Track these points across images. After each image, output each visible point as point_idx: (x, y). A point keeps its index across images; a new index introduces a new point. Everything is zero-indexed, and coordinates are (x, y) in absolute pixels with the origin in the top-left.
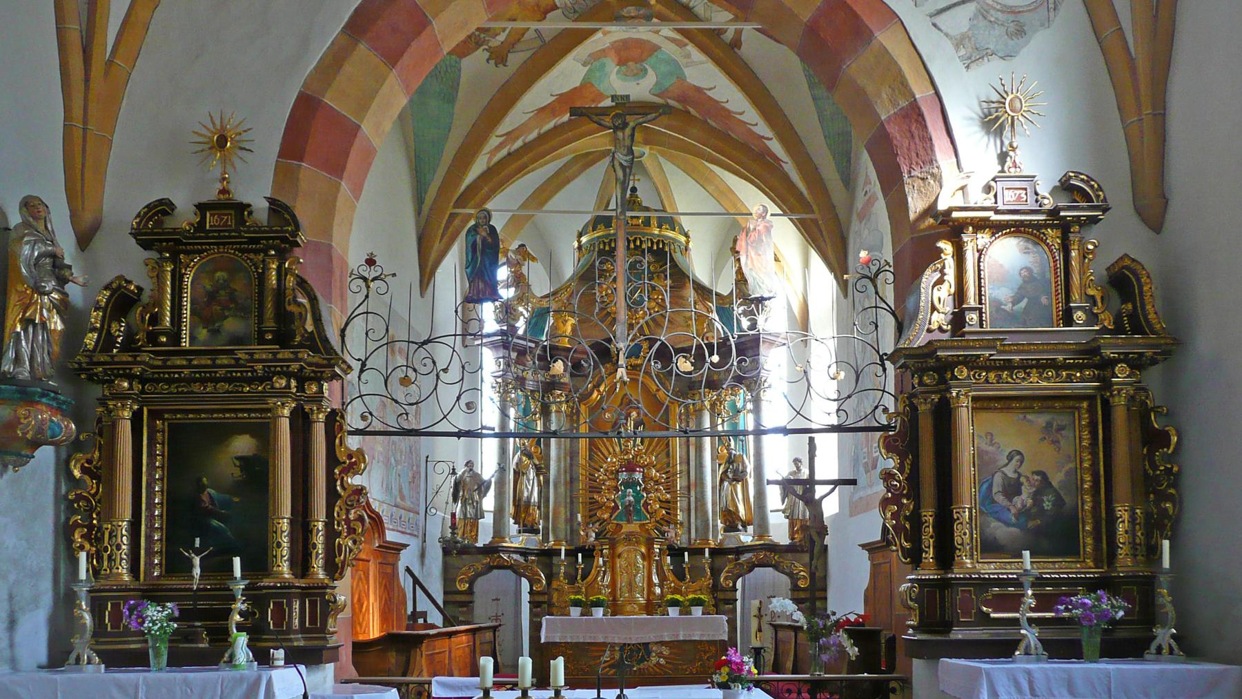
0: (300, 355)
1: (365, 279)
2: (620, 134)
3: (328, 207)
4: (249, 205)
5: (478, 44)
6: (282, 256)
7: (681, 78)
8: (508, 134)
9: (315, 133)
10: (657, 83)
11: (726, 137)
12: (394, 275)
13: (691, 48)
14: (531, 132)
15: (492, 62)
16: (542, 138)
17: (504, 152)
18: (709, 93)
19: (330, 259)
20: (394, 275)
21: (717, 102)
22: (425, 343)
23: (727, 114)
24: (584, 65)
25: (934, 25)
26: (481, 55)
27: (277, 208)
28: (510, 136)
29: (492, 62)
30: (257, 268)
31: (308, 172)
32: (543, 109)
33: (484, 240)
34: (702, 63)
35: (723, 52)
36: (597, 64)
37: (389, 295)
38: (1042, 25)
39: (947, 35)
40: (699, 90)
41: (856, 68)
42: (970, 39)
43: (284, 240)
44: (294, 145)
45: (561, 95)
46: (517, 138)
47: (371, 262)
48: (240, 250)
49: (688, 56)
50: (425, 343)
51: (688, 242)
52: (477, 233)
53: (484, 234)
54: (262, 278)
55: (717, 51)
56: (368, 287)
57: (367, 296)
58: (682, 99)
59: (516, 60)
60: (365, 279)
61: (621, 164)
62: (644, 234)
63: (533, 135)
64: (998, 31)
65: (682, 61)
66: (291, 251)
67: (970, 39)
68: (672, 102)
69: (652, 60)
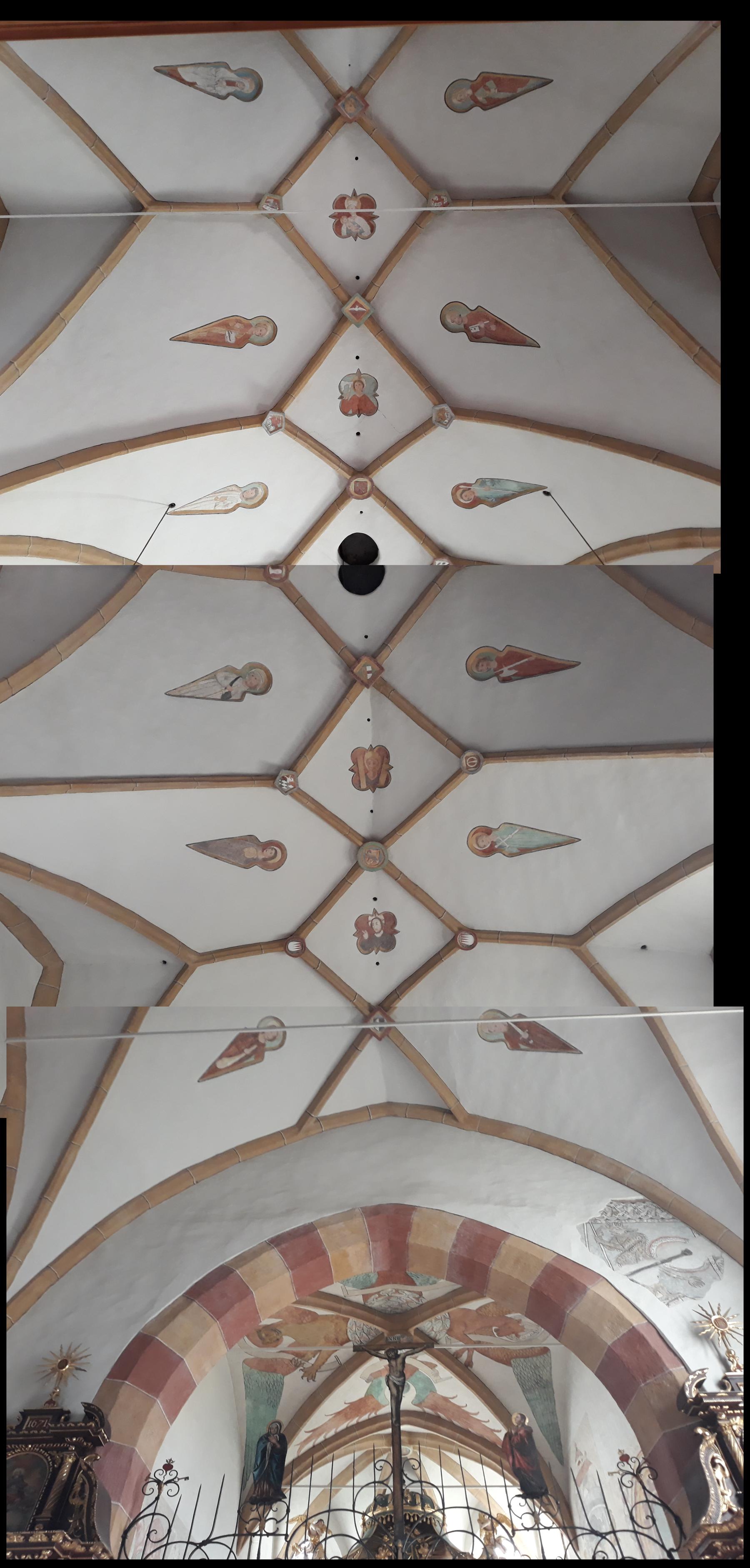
0: (54, 1538)
1: (159, 1482)
2: (393, 1363)
3: (139, 1420)
4: (69, 1412)
5: (297, 1366)
6: (82, 1451)
7: (433, 1391)
8: (313, 1431)
9: (147, 1363)
10: (417, 1396)
11: (466, 1433)
12: (187, 1478)
13: (440, 1368)
14: (330, 1429)
15: (305, 1378)
16: (338, 1436)
17: (310, 1445)
18: (452, 1401)
19: (130, 1461)
20: (187, 1478)
21: (459, 1407)
22: (205, 1543)
23: (467, 1415)
24: (367, 1381)
25: (632, 1280)
26: (298, 1373)
27: (92, 1412)
28: (315, 1432)
29: (305, 1378)
30: (54, 1463)
31: (128, 1390)
32: (339, 1413)
33: (274, 1447)
34: (448, 1378)
35: (463, 1370)
36: (376, 1381)
37: (178, 1496)
38: (715, 1278)
39: (644, 1286)
40: (446, 1399)
41: (578, 1312)
42: (663, 1288)
43: (87, 1437)
44: (123, 1368)
45: (351, 1404)
46: (320, 1435)
47: (168, 1467)
48: (46, 1450)
49: (437, 1374)
50: (205, 1543)
51: (444, 1518)
52: (268, 1440)
53: (274, 1441)
54: (56, 1471)
55: (457, 1368)
56: (160, 1489)
57: (157, 1498)
58: (434, 1407)
59: (321, 1377)
60: (159, 1482)
61: (395, 1384)
62: (412, 1511)
63: (332, 1433)
64: (682, 1283)
65: (433, 1379)
66: (93, 1450)
67: (663, 1288)
68: (428, 1410)
69: (413, 1378)
